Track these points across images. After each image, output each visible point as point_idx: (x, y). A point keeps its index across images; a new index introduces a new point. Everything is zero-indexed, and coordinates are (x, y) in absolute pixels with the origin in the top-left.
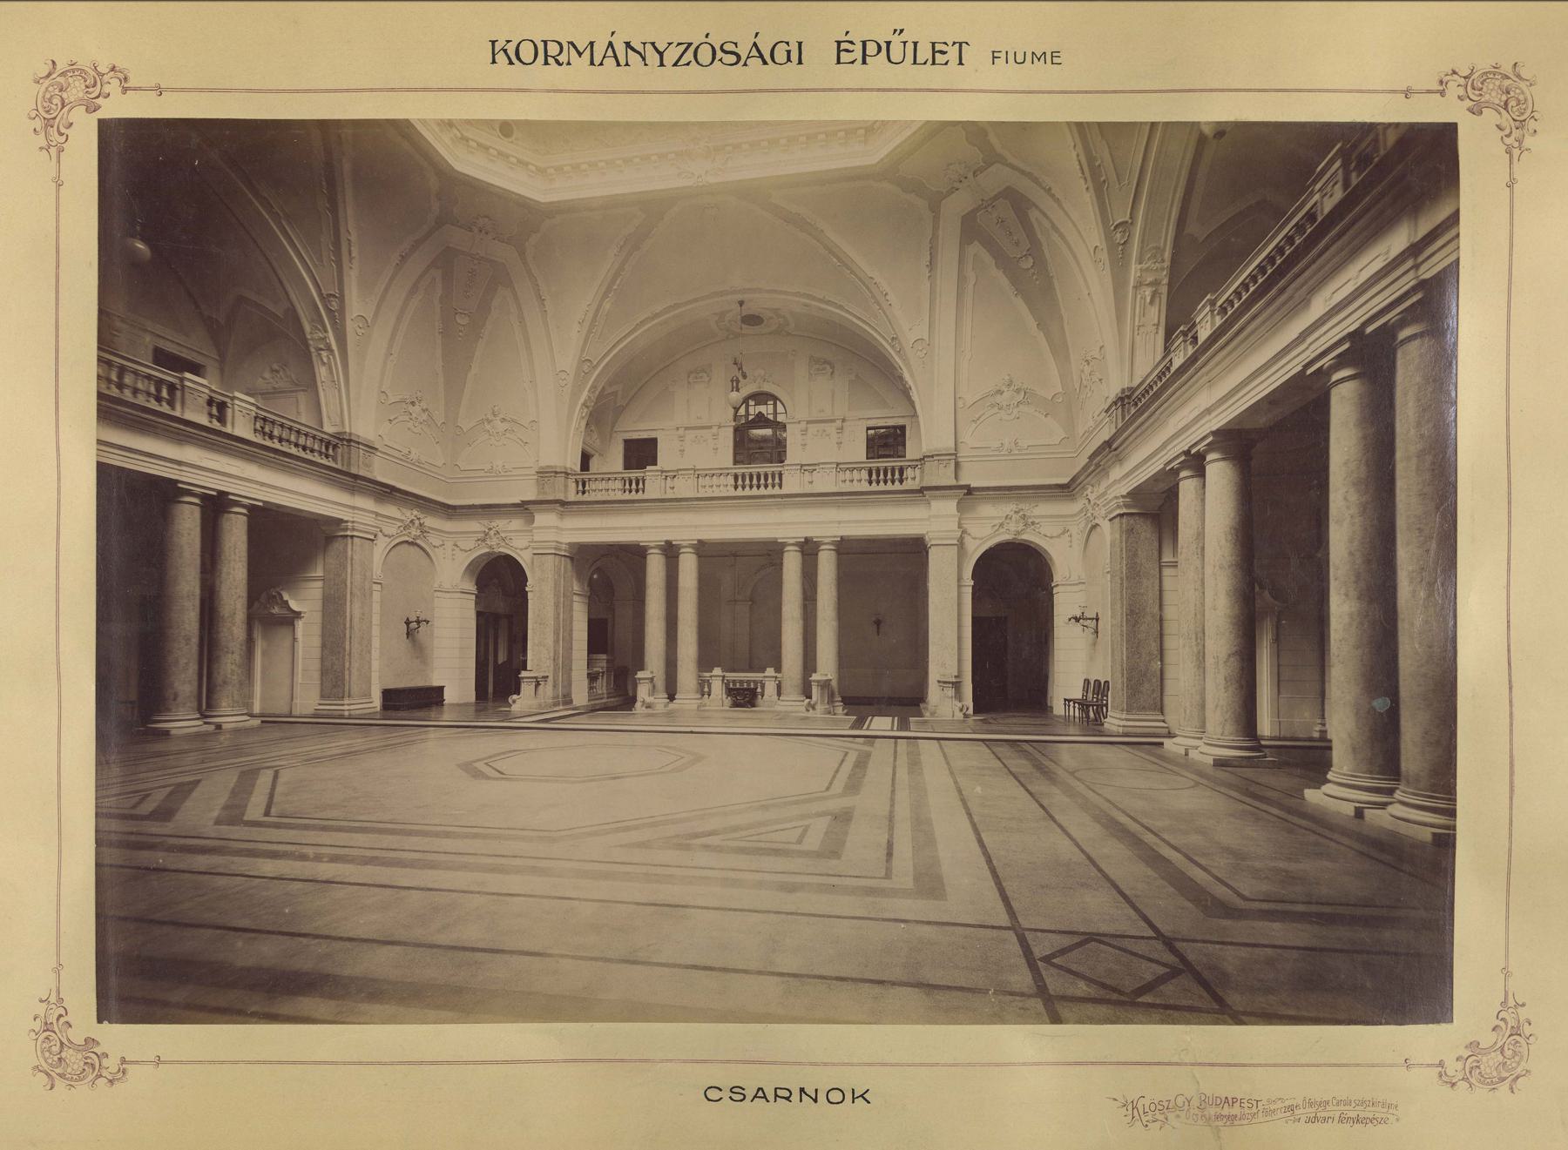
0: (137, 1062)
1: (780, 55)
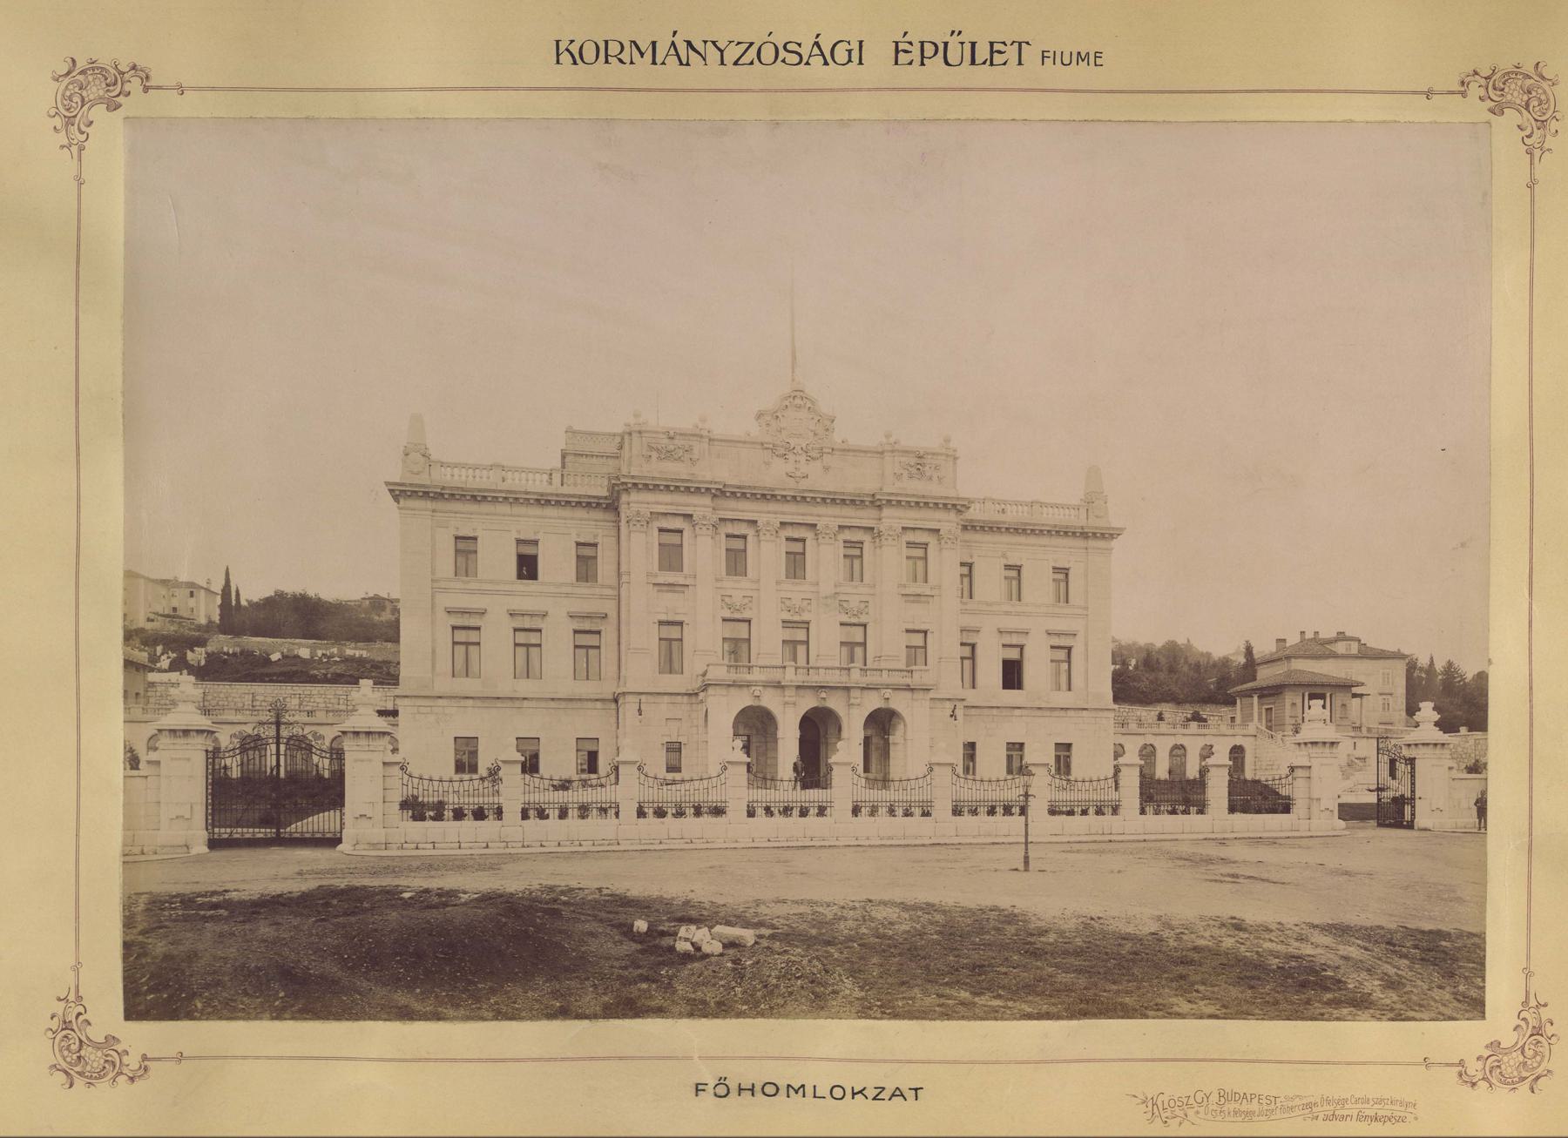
0: (159, 1059)
1: (841, 55)
